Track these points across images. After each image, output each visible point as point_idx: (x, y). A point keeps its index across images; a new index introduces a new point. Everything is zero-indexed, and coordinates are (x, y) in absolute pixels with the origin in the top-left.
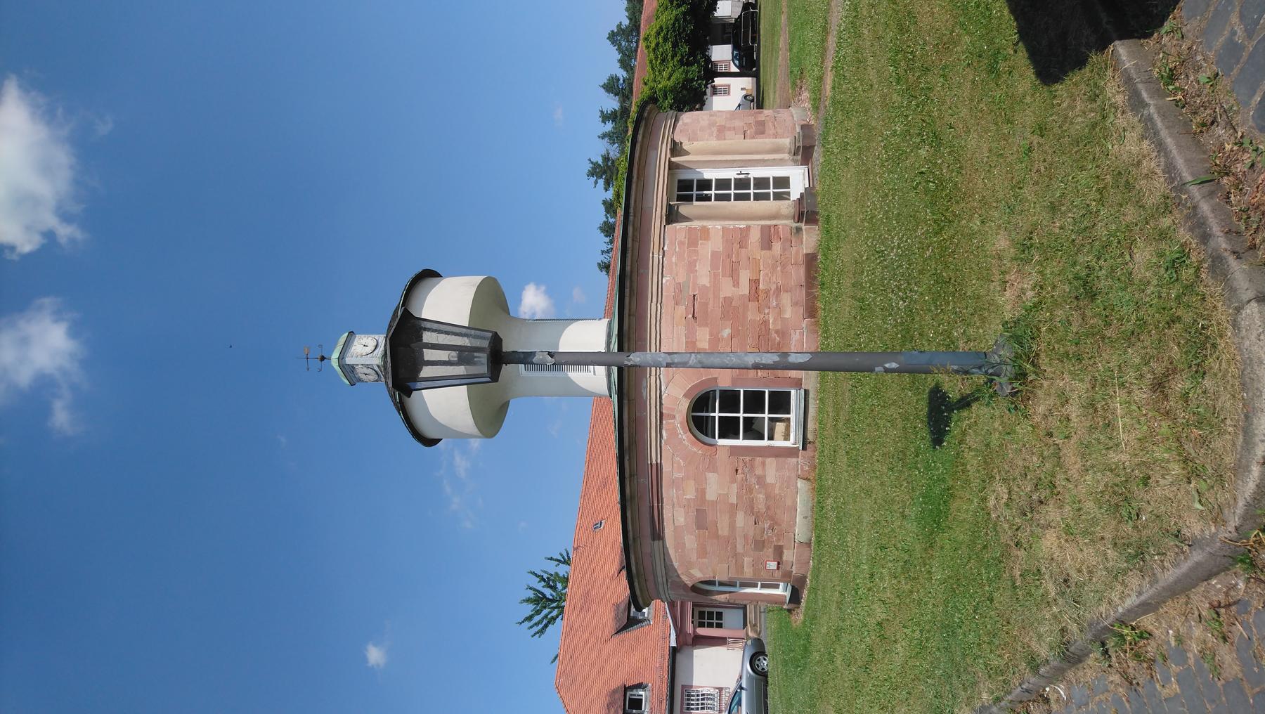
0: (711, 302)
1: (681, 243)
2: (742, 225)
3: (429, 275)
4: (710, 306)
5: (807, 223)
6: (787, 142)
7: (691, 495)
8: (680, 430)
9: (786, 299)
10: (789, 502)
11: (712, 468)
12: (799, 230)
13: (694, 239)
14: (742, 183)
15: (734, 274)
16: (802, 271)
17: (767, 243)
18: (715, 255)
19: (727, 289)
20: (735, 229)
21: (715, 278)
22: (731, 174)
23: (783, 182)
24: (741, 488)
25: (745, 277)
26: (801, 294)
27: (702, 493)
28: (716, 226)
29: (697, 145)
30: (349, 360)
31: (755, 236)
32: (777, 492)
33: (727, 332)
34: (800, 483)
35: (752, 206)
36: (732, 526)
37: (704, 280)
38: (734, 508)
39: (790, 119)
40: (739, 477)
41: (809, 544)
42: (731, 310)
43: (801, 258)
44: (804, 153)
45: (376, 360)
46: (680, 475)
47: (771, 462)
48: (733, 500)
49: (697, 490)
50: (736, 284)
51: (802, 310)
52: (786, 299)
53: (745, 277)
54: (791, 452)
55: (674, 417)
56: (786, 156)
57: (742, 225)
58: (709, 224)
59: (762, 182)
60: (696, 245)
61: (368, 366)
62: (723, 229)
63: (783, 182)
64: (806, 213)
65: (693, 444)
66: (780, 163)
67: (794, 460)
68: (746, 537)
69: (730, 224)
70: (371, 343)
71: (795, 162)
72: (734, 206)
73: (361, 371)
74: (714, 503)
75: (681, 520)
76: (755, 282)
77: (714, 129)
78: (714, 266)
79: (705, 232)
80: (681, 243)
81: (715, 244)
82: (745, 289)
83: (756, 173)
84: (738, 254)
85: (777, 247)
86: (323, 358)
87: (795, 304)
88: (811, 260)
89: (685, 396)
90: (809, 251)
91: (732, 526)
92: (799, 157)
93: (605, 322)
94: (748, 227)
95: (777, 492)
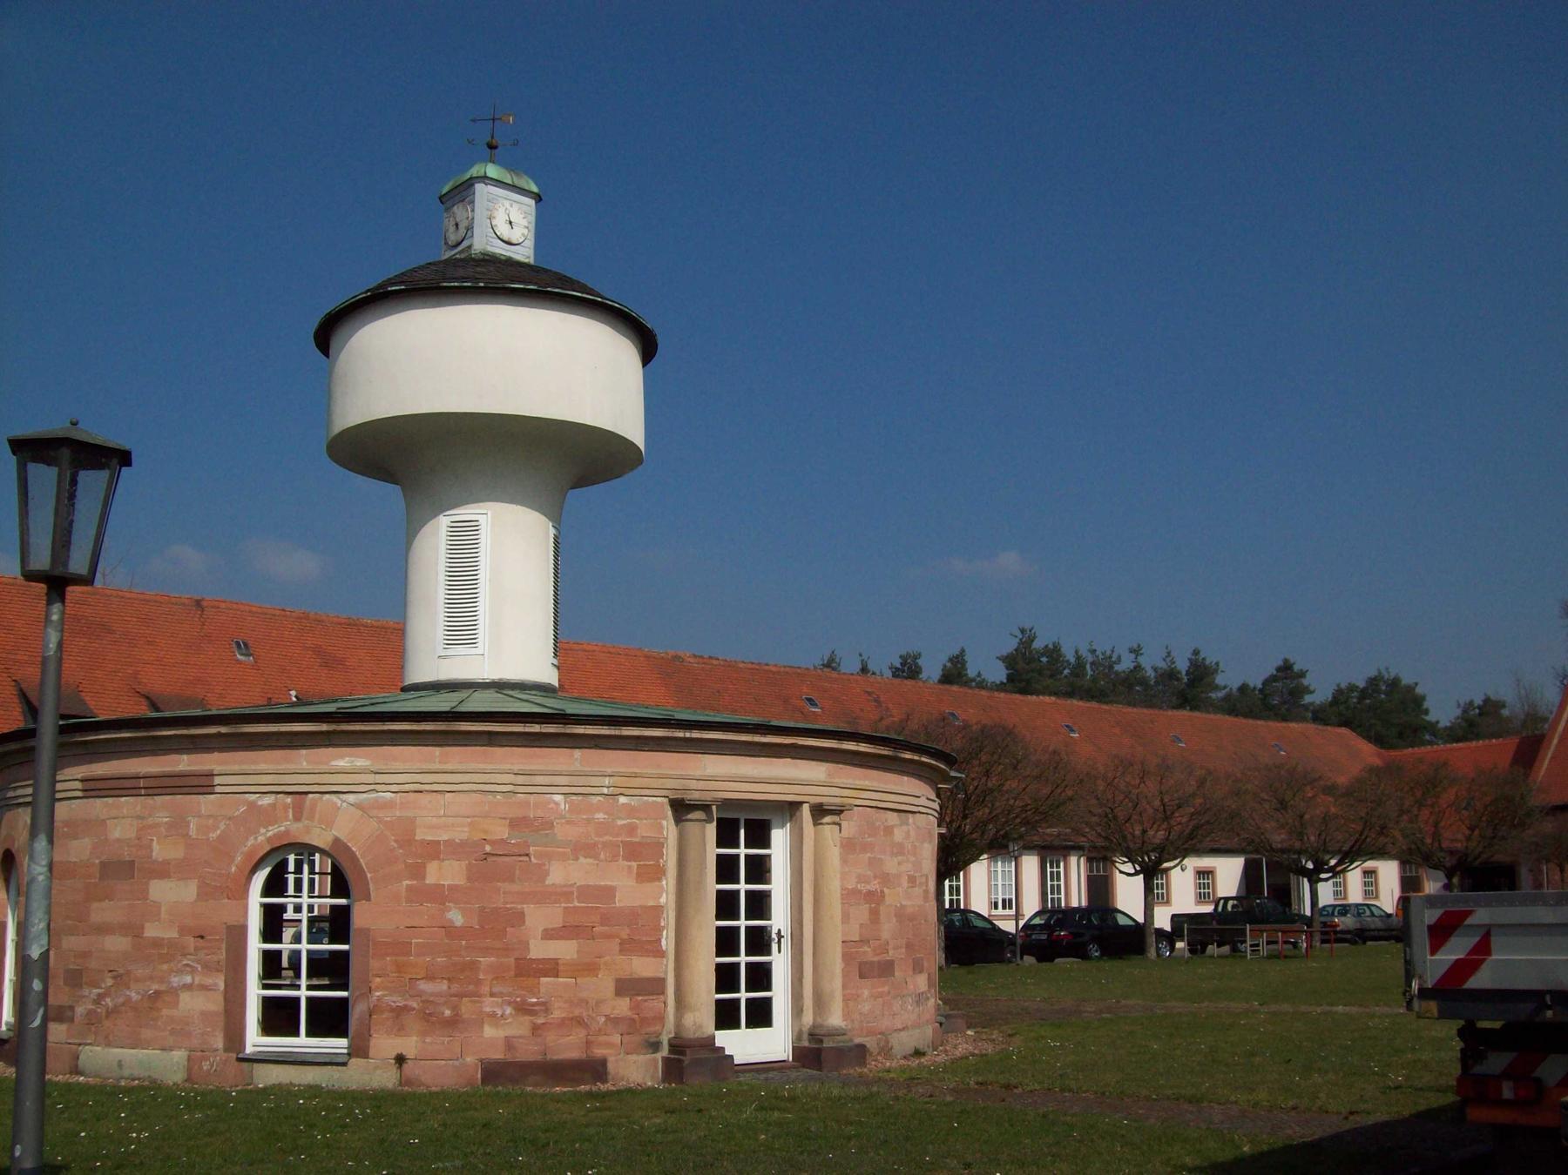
0: (516, 887)
1: (632, 829)
2: (667, 942)
3: (648, 348)
4: (506, 886)
5: (666, 1060)
6: (835, 1020)
7: (159, 851)
8: (272, 831)
9: (518, 1028)
10: (147, 1033)
11: (205, 893)
12: (655, 1046)
13: (644, 856)
14: (760, 941)
15: (567, 931)
16: (574, 1054)
17: (625, 987)
18: (609, 892)
19: (538, 918)
20: (659, 929)
21: (564, 894)
22: (779, 919)
23: (760, 1015)
24: (171, 943)
25: (565, 950)
26: (528, 1052)
27: (162, 871)
28: (666, 894)
29: (834, 854)
30: (479, 187)
31: (642, 967)
32: (165, 1012)
33: (456, 917)
34: (179, 1056)
35: (705, 960)
36: (104, 929)
37: (557, 875)
38: (133, 930)
39: (904, 1018)
40: (191, 942)
41: (76, 1071)
42: (498, 925)
43: (599, 1052)
44: (813, 1052)
45: (483, 242)
46: (193, 832)
47: (213, 1003)
48: (151, 931)
49: (166, 863)
50: (549, 935)
51: (498, 1055)
52: (518, 1028)
53: (565, 950)
54: (235, 1035)
55: (297, 818)
56: (808, 1019)
57: (667, 942)
58: (669, 882)
59: (760, 977)
60: (628, 858)
61: (470, 228)
62: (658, 910)
63: (760, 1015)
64: (689, 1059)
65: (249, 855)
66: (797, 1010)
67: (221, 1045)
68: (85, 955)
69: (669, 919)
70: (516, 235)
71: (798, 1037)
72: (707, 924)
73: (459, 211)
74: (144, 894)
75: (119, 831)
76: (551, 968)
77: (874, 886)
78: (586, 892)
79: (652, 874)
80: (632, 829)
81: (628, 891)
82: (539, 950)
83: (780, 963)
84: (609, 937)
85: (623, 1007)
86: (492, 147)
87: (509, 1043)
88: (596, 1069)
89: (337, 841)
90: (610, 1066)
91: (104, 929)
92: (806, 1044)
93: (551, 677)
94: (661, 954)
95: (165, 1012)
